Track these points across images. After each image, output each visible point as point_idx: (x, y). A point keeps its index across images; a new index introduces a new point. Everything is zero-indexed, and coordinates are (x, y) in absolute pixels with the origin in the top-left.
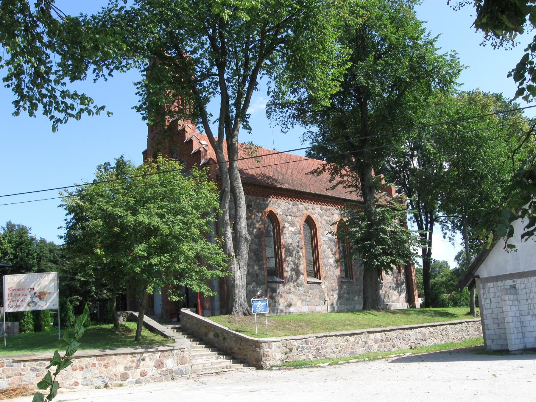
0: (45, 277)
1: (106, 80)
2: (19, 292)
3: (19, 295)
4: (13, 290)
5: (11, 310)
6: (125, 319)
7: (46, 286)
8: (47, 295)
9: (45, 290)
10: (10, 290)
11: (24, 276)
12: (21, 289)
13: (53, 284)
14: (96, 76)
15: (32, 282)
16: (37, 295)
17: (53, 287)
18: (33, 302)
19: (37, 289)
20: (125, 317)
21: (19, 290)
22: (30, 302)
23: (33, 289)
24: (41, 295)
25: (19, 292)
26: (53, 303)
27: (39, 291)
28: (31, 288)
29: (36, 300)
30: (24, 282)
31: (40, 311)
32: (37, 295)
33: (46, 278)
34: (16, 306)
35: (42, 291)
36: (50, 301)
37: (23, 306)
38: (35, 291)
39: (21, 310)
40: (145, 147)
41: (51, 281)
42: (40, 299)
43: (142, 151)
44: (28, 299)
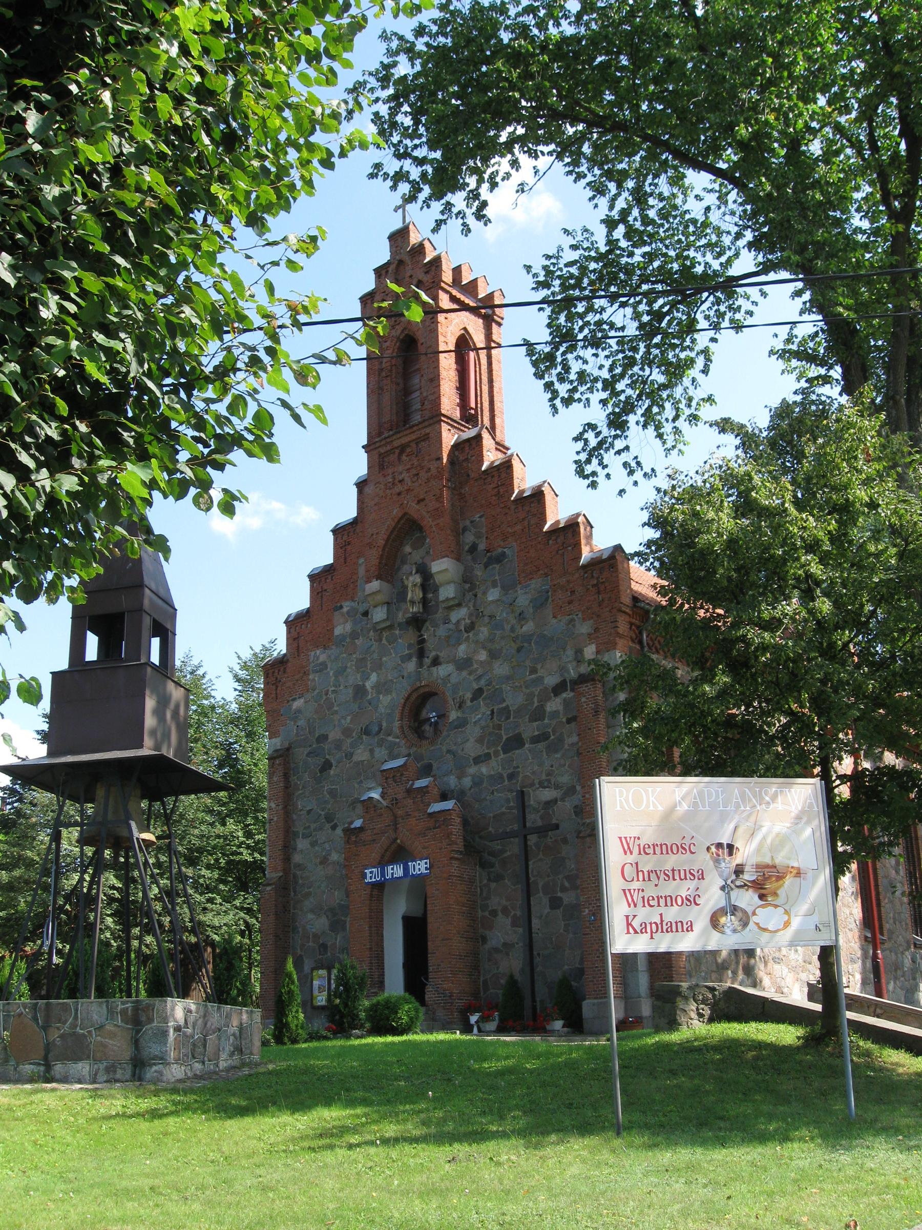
0: (774, 798)
1: (466, 230)
2: (671, 861)
3: (671, 875)
4: (643, 851)
5: (640, 945)
6: (707, 1012)
7: (782, 841)
8: (788, 881)
9: (780, 859)
10: (628, 851)
11: (685, 788)
12: (681, 848)
13: (808, 831)
14: (442, 213)
15: (724, 818)
16: (747, 877)
17: (811, 846)
18: (734, 909)
19: (746, 853)
20: (704, 1002)
21: (668, 853)
22: (722, 911)
23: (730, 847)
24: (766, 878)
25: (671, 861)
26: (815, 919)
27: (754, 860)
28: (719, 846)
29: (746, 899)
30: (689, 816)
31: (668, 955)
32: (747, 877)
33: (779, 805)
34: (663, 927)
35: (767, 860)
36: (804, 908)
37: (690, 928)
38: (738, 859)
39: (686, 943)
40: (348, 511)
41: (798, 818)
42: (762, 897)
43: (332, 527)
44: (713, 897)
